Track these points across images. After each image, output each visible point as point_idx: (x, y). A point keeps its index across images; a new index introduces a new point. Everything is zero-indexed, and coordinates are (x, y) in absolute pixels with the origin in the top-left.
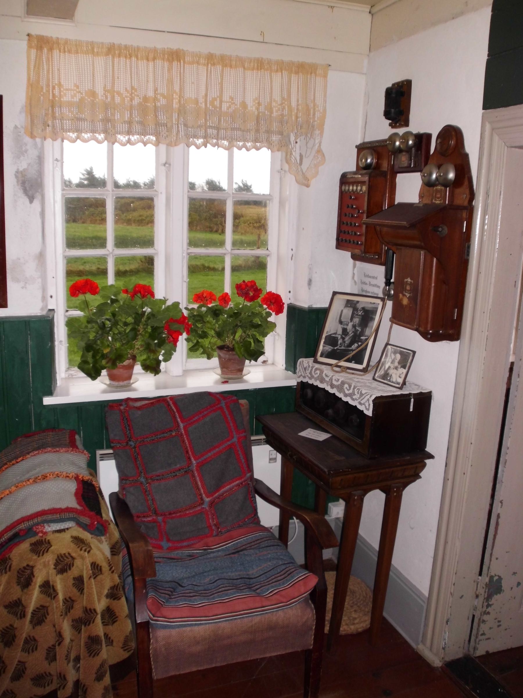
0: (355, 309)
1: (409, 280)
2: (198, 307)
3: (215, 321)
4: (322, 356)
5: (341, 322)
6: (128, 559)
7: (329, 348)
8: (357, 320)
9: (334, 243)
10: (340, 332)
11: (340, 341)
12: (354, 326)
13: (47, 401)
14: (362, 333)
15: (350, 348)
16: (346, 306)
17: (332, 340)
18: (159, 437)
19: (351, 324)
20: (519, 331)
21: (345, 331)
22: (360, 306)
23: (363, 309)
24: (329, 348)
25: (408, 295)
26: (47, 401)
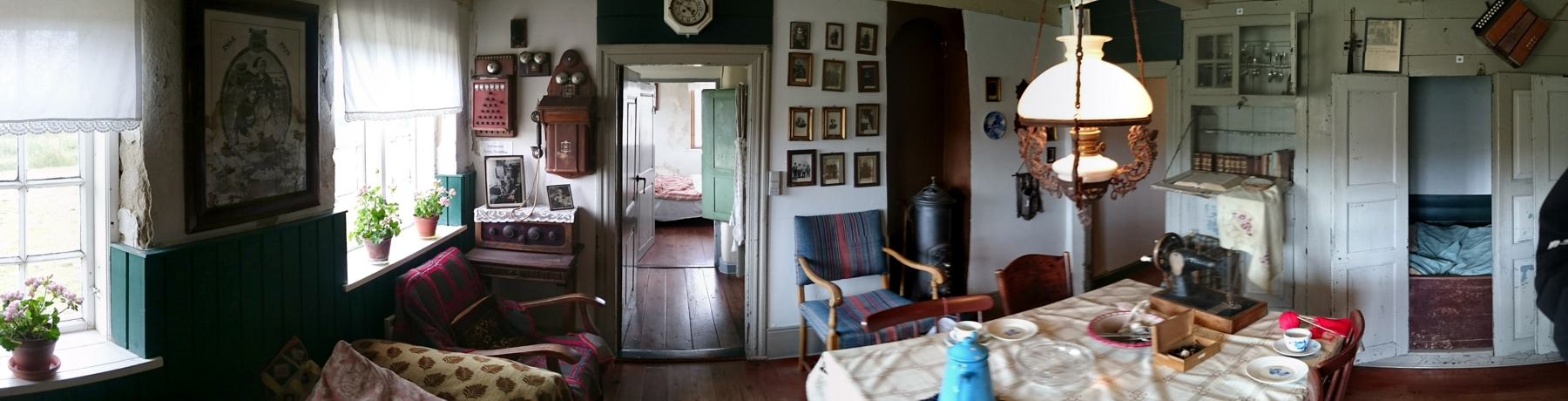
0: (505, 166)
1: (566, 142)
2: (527, 234)
3: (1156, 241)
4: (491, 203)
5: (498, 177)
6: (883, 309)
7: (495, 197)
8: (509, 174)
9: (860, 21)
10: (500, 184)
11: (502, 191)
12: (508, 178)
13: (1108, 39)
14: (516, 182)
15: (513, 191)
16: (497, 165)
17: (495, 191)
18: (1211, 265)
19: (506, 178)
20: (1349, 40)
21: (502, 182)
22: (507, 163)
23: (510, 165)
24: (495, 197)
25: (566, 152)
26: (1108, 39)
